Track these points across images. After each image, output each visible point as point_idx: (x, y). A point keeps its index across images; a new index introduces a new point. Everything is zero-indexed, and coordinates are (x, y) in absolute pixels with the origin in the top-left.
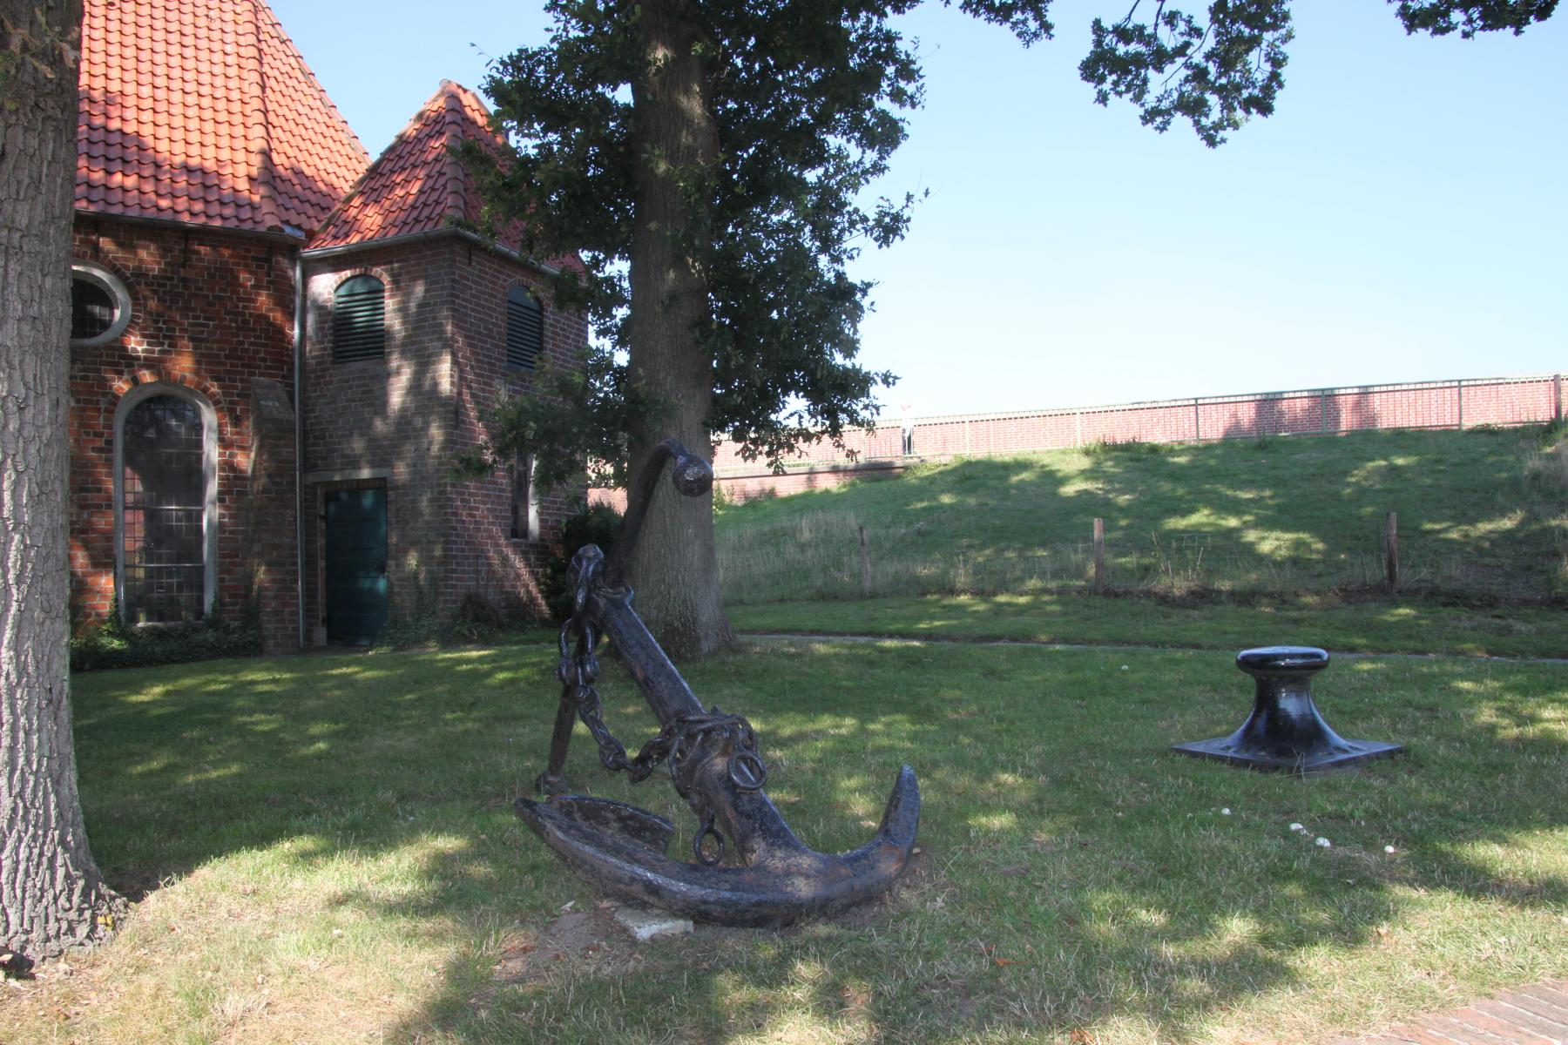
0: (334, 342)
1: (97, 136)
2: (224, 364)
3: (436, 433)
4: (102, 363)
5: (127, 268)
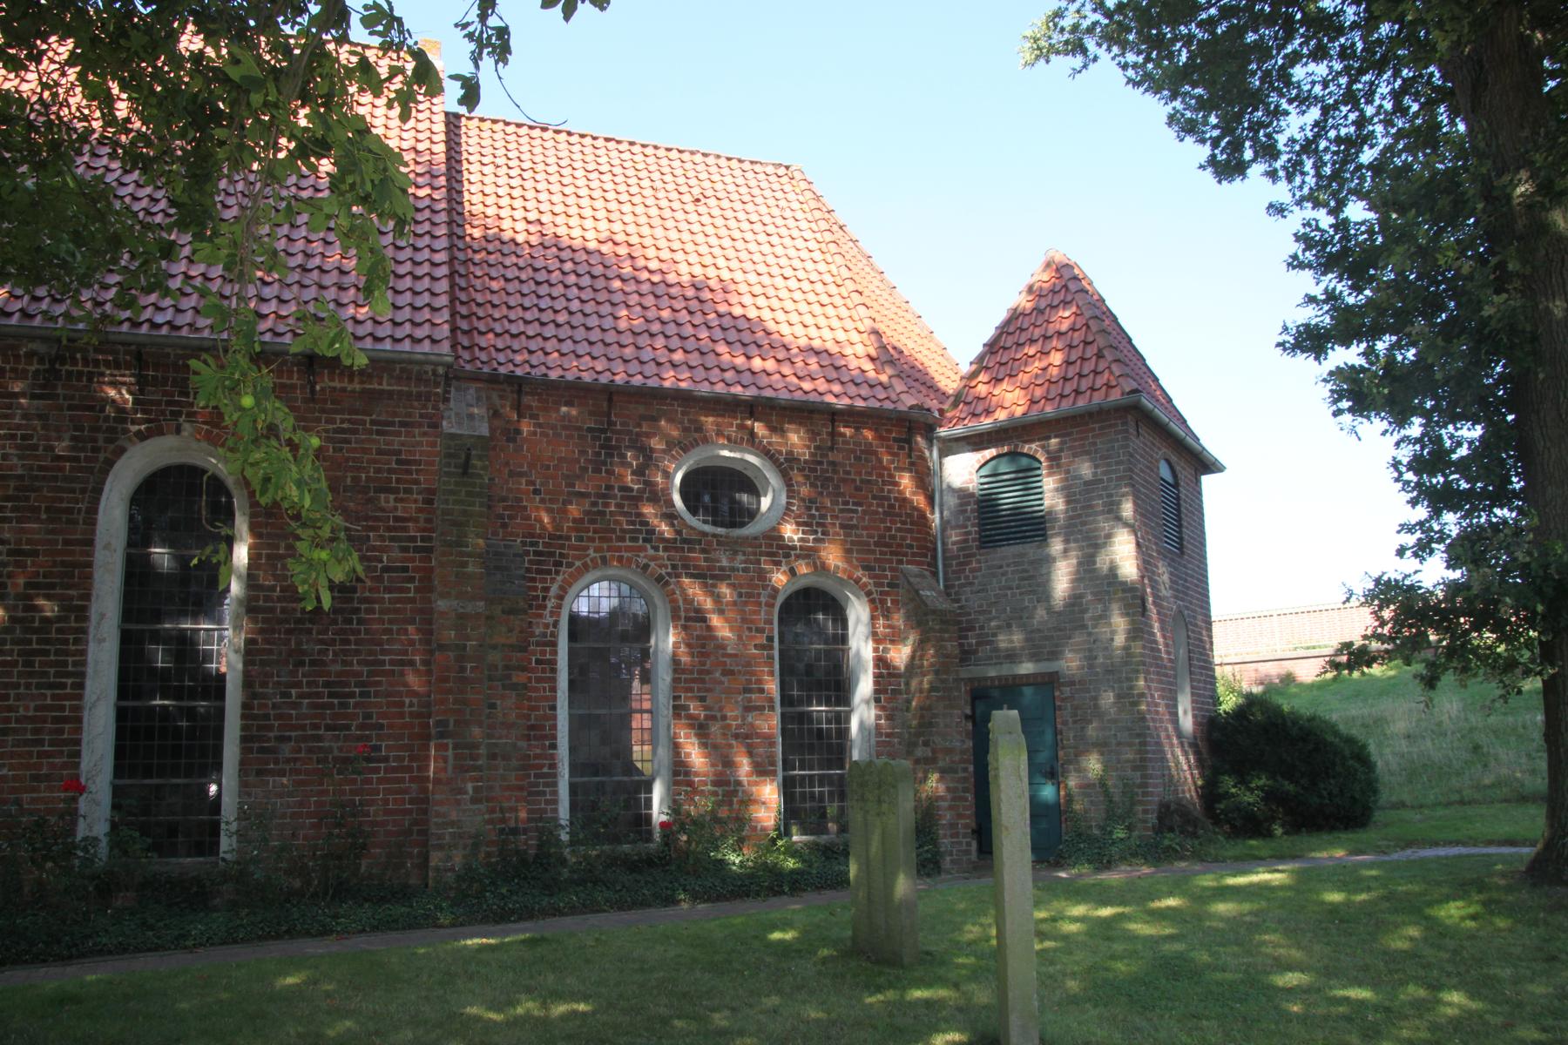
0: (979, 525)
1: (727, 322)
2: (874, 552)
3: (1119, 624)
4: (761, 554)
5: (780, 453)
